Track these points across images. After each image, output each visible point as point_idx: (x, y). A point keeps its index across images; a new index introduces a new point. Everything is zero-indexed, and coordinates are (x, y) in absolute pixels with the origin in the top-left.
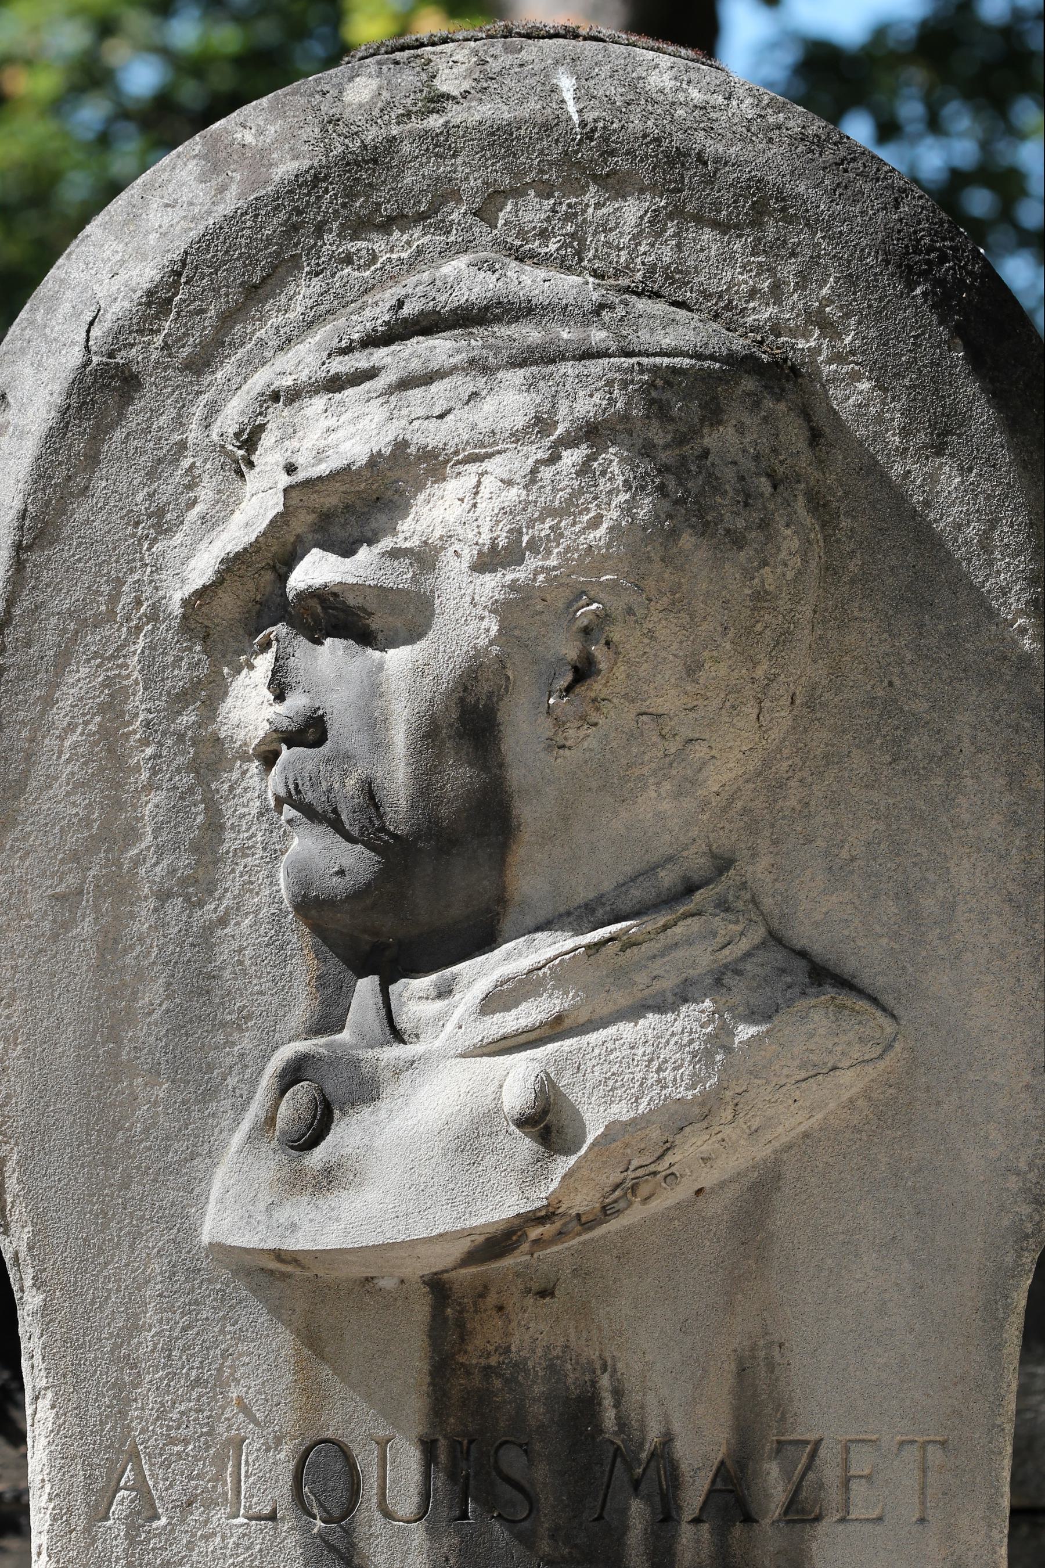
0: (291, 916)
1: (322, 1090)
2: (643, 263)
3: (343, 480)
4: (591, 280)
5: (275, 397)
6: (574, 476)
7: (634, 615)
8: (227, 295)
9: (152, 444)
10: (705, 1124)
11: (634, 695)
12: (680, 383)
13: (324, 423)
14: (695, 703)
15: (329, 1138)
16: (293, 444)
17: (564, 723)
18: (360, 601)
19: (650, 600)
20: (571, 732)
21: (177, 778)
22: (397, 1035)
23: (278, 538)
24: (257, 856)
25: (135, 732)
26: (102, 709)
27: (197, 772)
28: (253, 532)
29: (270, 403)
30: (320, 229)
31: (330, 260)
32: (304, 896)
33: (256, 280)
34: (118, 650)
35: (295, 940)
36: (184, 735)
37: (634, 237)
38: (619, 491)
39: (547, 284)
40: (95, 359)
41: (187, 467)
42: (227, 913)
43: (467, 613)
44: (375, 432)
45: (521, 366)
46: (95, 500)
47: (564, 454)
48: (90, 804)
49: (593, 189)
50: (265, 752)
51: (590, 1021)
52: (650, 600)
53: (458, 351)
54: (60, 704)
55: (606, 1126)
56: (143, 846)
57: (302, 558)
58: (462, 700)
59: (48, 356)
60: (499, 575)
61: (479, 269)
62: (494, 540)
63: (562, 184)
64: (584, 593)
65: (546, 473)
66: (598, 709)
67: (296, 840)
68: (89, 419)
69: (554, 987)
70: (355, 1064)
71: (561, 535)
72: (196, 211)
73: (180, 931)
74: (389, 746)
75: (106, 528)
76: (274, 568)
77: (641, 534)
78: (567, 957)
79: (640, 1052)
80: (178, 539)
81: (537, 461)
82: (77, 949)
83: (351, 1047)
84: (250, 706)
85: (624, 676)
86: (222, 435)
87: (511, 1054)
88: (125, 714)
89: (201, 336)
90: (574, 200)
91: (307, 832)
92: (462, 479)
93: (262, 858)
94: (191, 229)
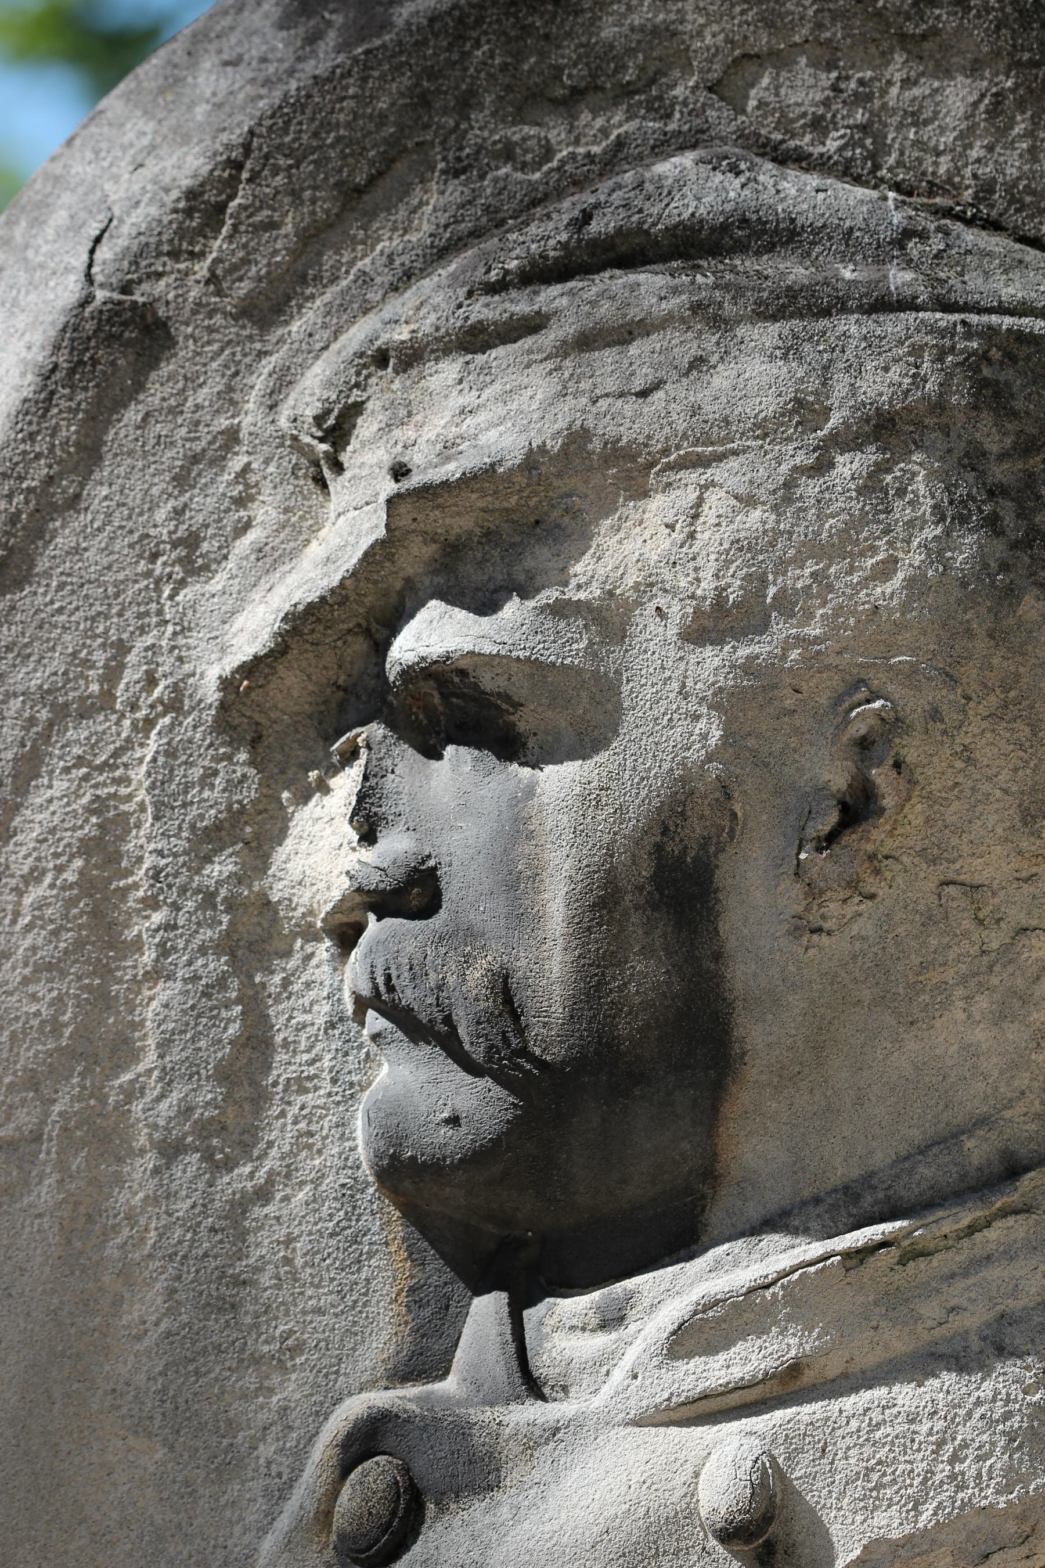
0: (371, 1190)
1: (408, 1470)
2: (975, 176)
3: (481, 490)
4: (891, 195)
5: (381, 359)
6: (854, 494)
7: (942, 721)
8: (313, 201)
9: (183, 431)
10: (1024, 1550)
11: (936, 851)
12: (1028, 358)
13: (457, 401)
14: (1034, 870)
15: (417, 1548)
16: (409, 433)
17: (822, 892)
18: (501, 683)
19: (968, 699)
20: (833, 908)
21: (200, 962)
22: (532, 1385)
23: (376, 582)
24: (322, 1092)
25: (136, 886)
26: (86, 847)
27: (233, 955)
28: (336, 571)
29: (372, 368)
30: (466, 103)
31: (478, 152)
32: (394, 1157)
33: (360, 179)
34: (116, 754)
35: (375, 1228)
36: (214, 895)
37: (961, 136)
38: (925, 522)
39: (821, 196)
40: (100, 295)
41: (238, 469)
42: (270, 1181)
43: (672, 709)
44: (535, 416)
45: (774, 318)
46: (89, 517)
47: (840, 459)
48: (60, 999)
49: (899, 58)
50: (342, 925)
51: (845, 1375)
52: (968, 699)
53: (675, 291)
54: (19, 838)
55: (865, 1547)
56: (141, 1068)
57: (412, 616)
58: (659, 848)
59: (28, 292)
60: (727, 648)
61: (714, 169)
62: (720, 591)
63: (851, 47)
64: (862, 681)
65: (810, 488)
66: (877, 872)
67: (385, 1068)
68: (86, 389)
69: (789, 1318)
70: (463, 1430)
71: (830, 588)
72: (271, 70)
73: (193, 1207)
74: (539, 918)
75: (105, 562)
76: (368, 632)
77: (957, 592)
78: (812, 1269)
79: (924, 1429)
80: (218, 582)
81: (795, 469)
82: (28, 1229)
83: (459, 1403)
84: (321, 853)
85: (920, 820)
86: (295, 420)
87: (715, 1423)
88: (122, 857)
89: (269, 264)
90: (869, 74)
91: (402, 1054)
92: (674, 494)
93: (329, 1095)
94: (261, 97)
